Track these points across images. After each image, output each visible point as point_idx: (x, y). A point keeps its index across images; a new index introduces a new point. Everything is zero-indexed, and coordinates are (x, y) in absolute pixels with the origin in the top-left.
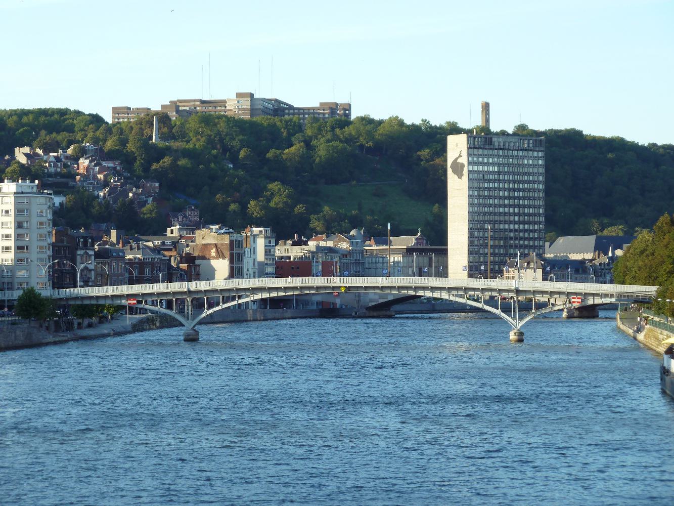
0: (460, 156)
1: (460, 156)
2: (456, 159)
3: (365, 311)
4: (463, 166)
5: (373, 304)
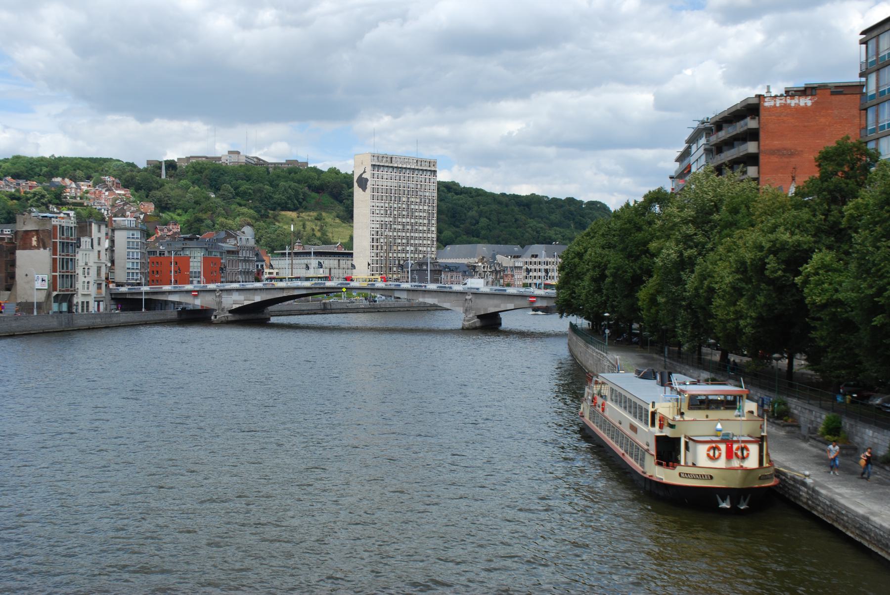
0: (364, 172)
1: (364, 172)
2: (362, 175)
3: (228, 314)
4: (367, 180)
5: (237, 306)
